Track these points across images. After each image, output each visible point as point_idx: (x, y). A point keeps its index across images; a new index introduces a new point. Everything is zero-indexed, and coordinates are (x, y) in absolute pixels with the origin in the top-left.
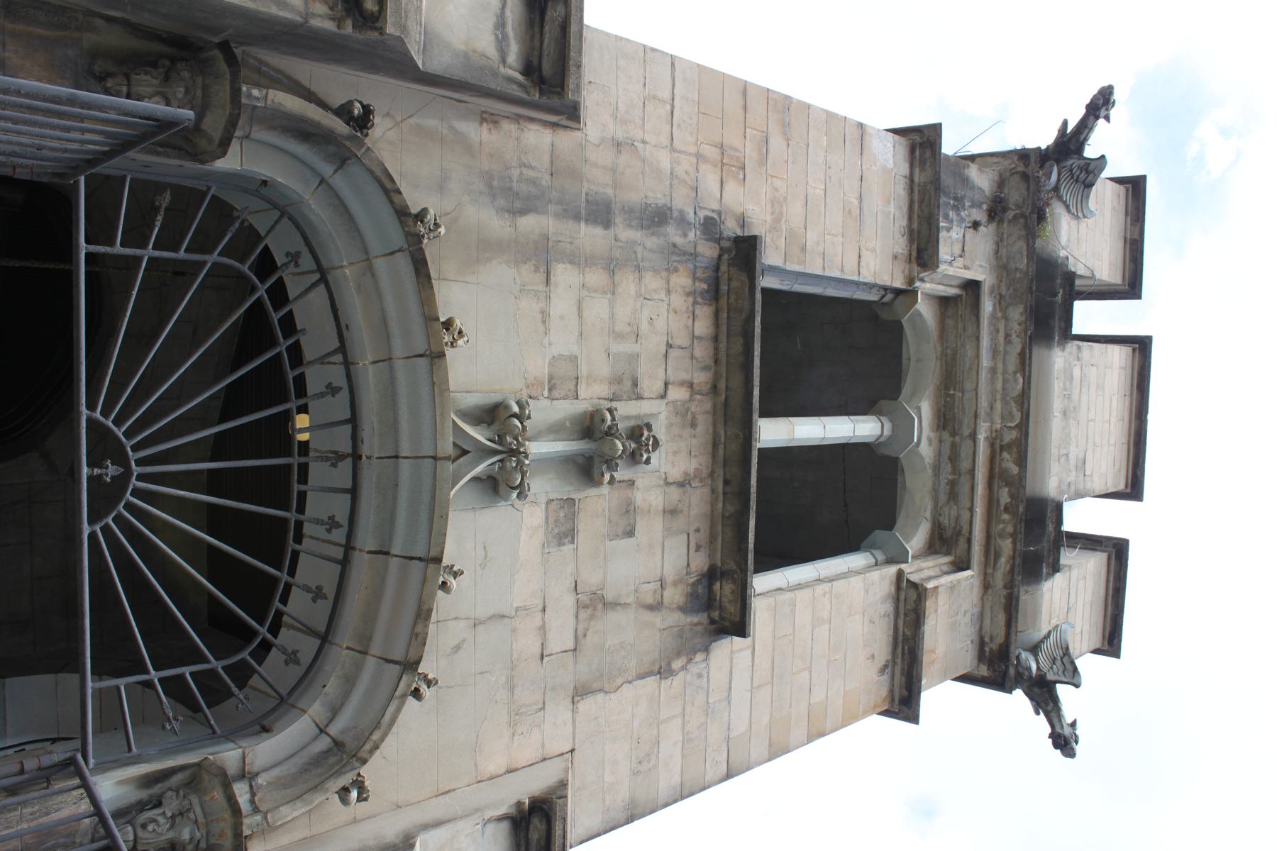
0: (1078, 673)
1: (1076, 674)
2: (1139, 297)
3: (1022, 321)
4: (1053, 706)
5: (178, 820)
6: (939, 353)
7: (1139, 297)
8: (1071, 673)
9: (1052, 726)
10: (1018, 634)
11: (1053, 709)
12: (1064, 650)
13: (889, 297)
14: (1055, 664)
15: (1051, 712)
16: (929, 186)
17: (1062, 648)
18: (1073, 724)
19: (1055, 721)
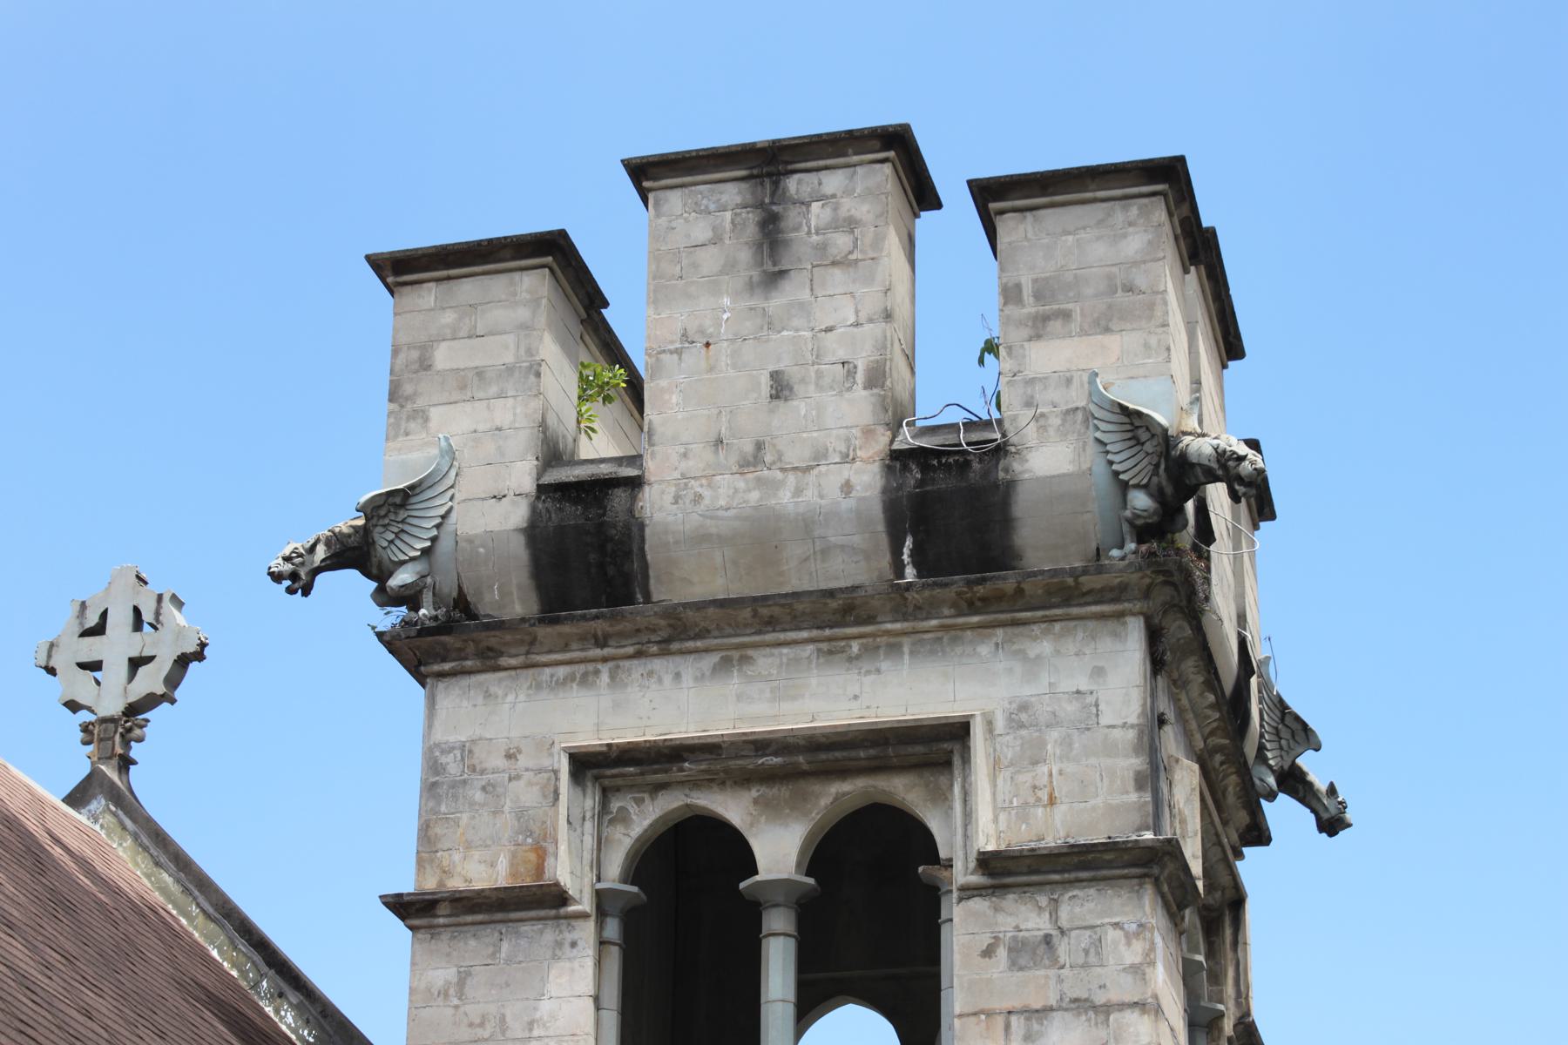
0: (1310, 729)
1: (1309, 733)
2: (1180, 161)
3: (448, 983)
4: (1303, 787)
5: (478, 1021)
6: (1028, 358)
7: (1180, 161)
8: (1303, 734)
9: (1313, 811)
10: (767, 181)
11: (1305, 791)
12: (1278, 705)
13: (1240, 489)
14: (1281, 738)
15: (1305, 797)
16: (1256, 833)
17: (1276, 706)
18: (1332, 790)
19: (1314, 803)
